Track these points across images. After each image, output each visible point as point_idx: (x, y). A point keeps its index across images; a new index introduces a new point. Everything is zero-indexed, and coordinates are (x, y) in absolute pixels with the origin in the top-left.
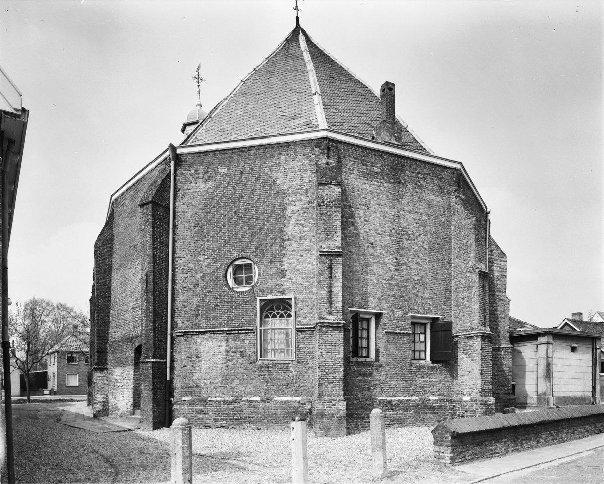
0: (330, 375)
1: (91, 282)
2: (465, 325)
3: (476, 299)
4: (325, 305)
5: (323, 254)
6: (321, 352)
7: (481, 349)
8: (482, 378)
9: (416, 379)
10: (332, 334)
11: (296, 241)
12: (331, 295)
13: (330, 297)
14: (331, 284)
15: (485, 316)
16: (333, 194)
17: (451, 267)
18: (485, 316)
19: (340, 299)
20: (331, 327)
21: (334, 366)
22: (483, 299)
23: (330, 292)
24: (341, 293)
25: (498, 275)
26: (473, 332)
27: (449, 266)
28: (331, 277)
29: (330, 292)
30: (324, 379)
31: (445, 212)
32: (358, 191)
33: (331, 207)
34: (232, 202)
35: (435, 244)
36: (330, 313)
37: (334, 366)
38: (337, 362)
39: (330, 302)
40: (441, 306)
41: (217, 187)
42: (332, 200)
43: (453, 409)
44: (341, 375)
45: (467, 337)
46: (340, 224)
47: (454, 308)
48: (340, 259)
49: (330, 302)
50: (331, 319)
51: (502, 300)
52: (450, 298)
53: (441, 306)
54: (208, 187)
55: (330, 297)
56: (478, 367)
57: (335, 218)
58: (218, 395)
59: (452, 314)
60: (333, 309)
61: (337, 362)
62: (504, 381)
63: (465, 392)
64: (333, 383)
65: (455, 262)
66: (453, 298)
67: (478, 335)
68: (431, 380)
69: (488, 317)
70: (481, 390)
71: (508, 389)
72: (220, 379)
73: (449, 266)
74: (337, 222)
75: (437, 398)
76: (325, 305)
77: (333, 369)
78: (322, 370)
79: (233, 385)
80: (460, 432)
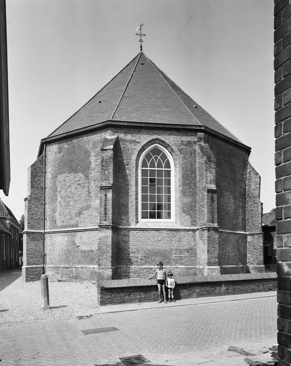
0: (104, 254)
1: (275, 174)
2: (201, 222)
3: (206, 206)
4: (103, 216)
5: (101, 188)
6: (100, 242)
7: (208, 237)
8: (208, 255)
9: (170, 255)
10: (105, 232)
11: (98, 181)
12: (106, 210)
13: (105, 211)
14: (106, 204)
15: (213, 217)
16: (108, 155)
17: (196, 187)
18: (213, 217)
19: (111, 212)
20: (105, 228)
21: (106, 249)
22: (212, 206)
23: (105, 209)
24: (111, 209)
25: (254, 187)
26: (204, 227)
27: (194, 186)
28: (106, 201)
29: (105, 209)
30: (101, 256)
31: (191, 155)
32: (132, 150)
33: (108, 162)
34: (70, 163)
35: (185, 174)
36: (105, 220)
37: (106, 249)
38: (108, 247)
39: (106, 214)
40: (188, 211)
41: (63, 155)
42: (108, 158)
43: (196, 273)
44: (110, 254)
45: (202, 230)
46: (112, 171)
47: (197, 212)
48: (111, 190)
49: (106, 214)
50: (105, 223)
51: (256, 203)
52: (195, 206)
53: (188, 211)
54: (60, 156)
55: (105, 211)
56: (206, 248)
57: (110, 168)
58: (63, 264)
59: (197, 216)
60: (107, 218)
61: (108, 247)
62: (257, 256)
63: (201, 263)
64: (106, 258)
65: (198, 185)
66: (197, 206)
67: (206, 228)
68: (180, 256)
69: (216, 217)
70: (207, 262)
71: (260, 261)
72: (64, 256)
73: (194, 186)
74: (111, 170)
75: (184, 267)
76: (103, 216)
77: (106, 251)
78: (100, 251)
79: (70, 259)
80: (107, 287)
